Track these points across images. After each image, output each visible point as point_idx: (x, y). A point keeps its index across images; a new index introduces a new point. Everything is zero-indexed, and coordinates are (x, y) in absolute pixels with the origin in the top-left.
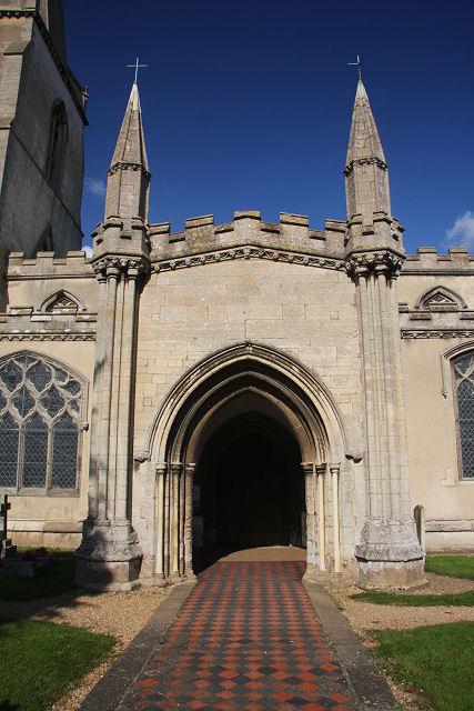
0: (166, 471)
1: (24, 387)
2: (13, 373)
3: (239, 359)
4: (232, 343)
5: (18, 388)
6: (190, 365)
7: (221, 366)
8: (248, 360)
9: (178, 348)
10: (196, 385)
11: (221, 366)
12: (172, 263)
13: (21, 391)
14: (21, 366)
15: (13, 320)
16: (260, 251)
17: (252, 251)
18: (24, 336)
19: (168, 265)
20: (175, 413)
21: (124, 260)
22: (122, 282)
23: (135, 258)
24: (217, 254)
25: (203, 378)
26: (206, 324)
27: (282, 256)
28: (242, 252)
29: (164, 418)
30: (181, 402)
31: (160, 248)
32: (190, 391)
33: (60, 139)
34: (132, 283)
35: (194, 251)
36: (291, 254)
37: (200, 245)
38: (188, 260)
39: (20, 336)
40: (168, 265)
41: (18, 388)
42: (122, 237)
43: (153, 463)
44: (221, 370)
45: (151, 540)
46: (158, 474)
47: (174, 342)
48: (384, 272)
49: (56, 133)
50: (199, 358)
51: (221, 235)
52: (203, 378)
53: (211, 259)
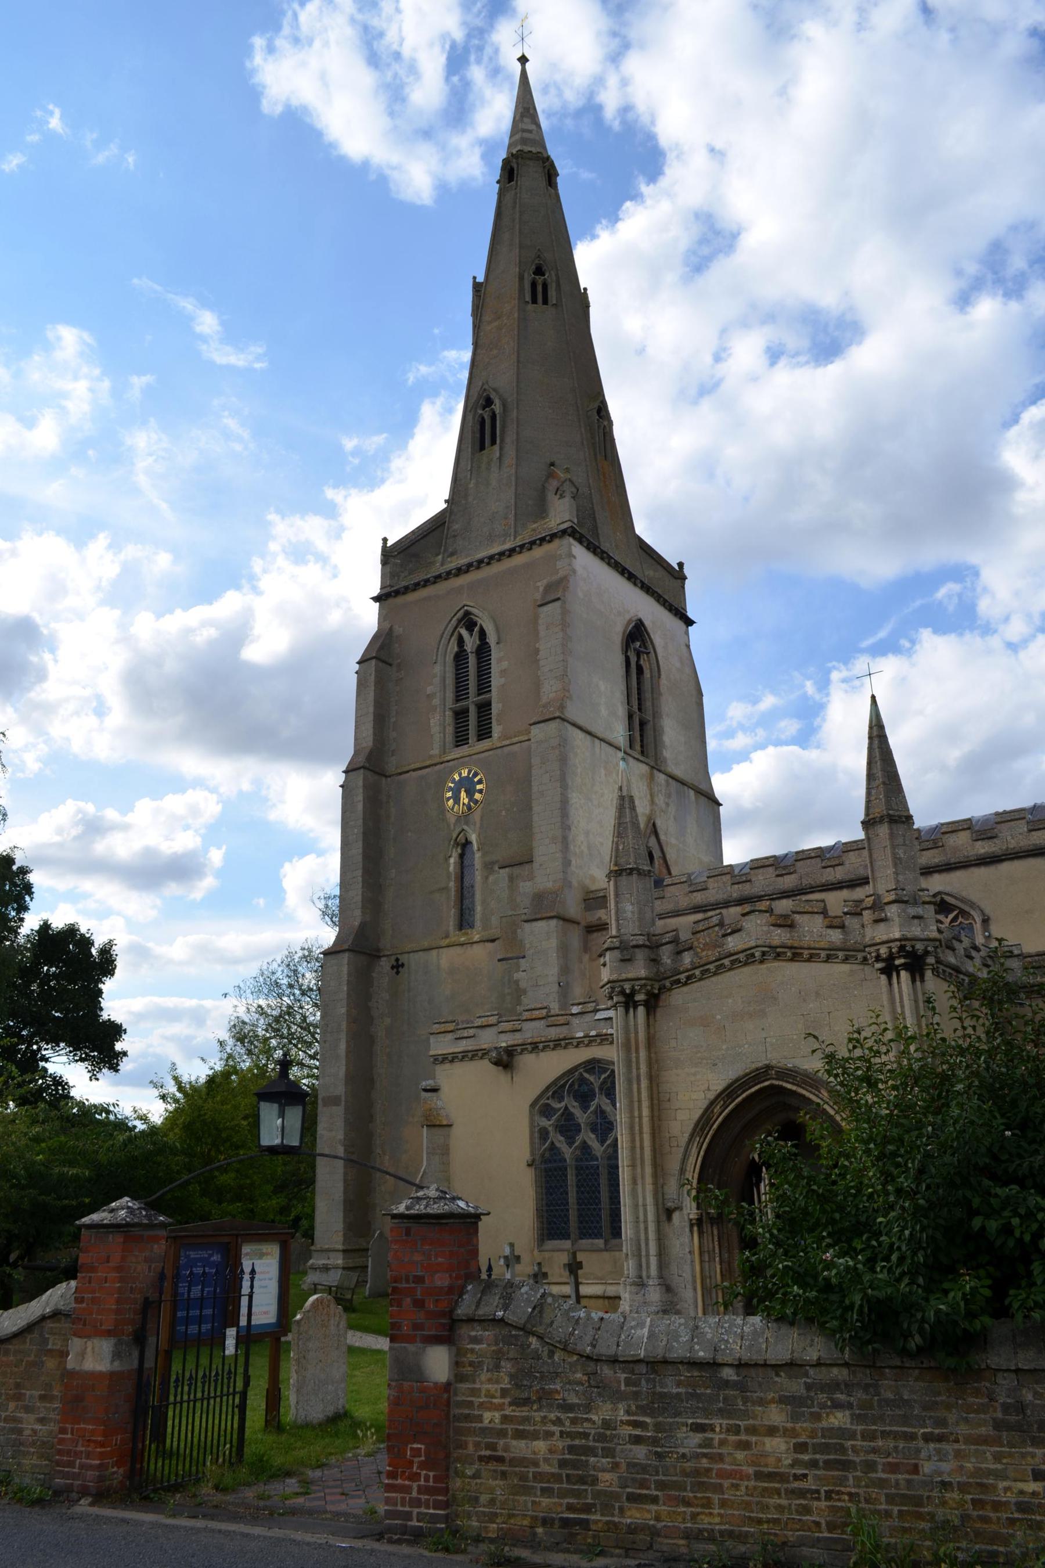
0: (699, 1222)
1: (599, 1106)
2: (585, 1088)
3: (762, 1085)
4: (754, 1066)
5: (592, 1109)
6: (711, 1096)
7: (744, 1095)
8: (772, 1086)
9: (698, 1077)
10: (720, 1119)
11: (744, 1095)
12: (683, 977)
13: (595, 1112)
14: (592, 1079)
15: (575, 1021)
16: (775, 953)
17: (764, 954)
18: (589, 1041)
19: (678, 981)
20: (702, 1153)
21: (627, 987)
22: (631, 1010)
23: (637, 983)
24: (726, 962)
25: (727, 1111)
26: (724, 1047)
27: (796, 955)
28: (753, 955)
29: (692, 1160)
30: (707, 1140)
31: (669, 961)
32: (715, 1126)
33: (647, 674)
34: (641, 1010)
35: (703, 962)
36: (806, 952)
37: (712, 954)
38: (697, 972)
39: (586, 1040)
40: (678, 981)
41: (592, 1109)
42: (622, 960)
43: (685, 1212)
44: (744, 1100)
45: (691, 1301)
46: (692, 1226)
47: (693, 1070)
48: (905, 967)
49: (640, 670)
50: (720, 1088)
51: (730, 939)
52: (727, 1111)
53: (720, 970)
